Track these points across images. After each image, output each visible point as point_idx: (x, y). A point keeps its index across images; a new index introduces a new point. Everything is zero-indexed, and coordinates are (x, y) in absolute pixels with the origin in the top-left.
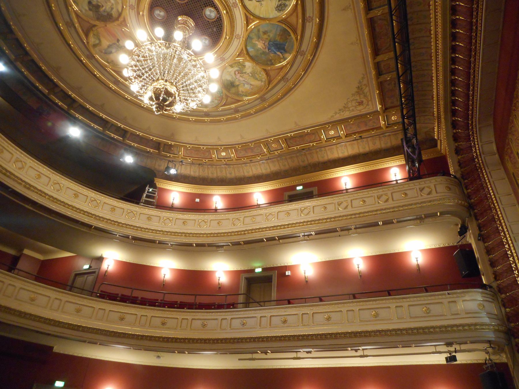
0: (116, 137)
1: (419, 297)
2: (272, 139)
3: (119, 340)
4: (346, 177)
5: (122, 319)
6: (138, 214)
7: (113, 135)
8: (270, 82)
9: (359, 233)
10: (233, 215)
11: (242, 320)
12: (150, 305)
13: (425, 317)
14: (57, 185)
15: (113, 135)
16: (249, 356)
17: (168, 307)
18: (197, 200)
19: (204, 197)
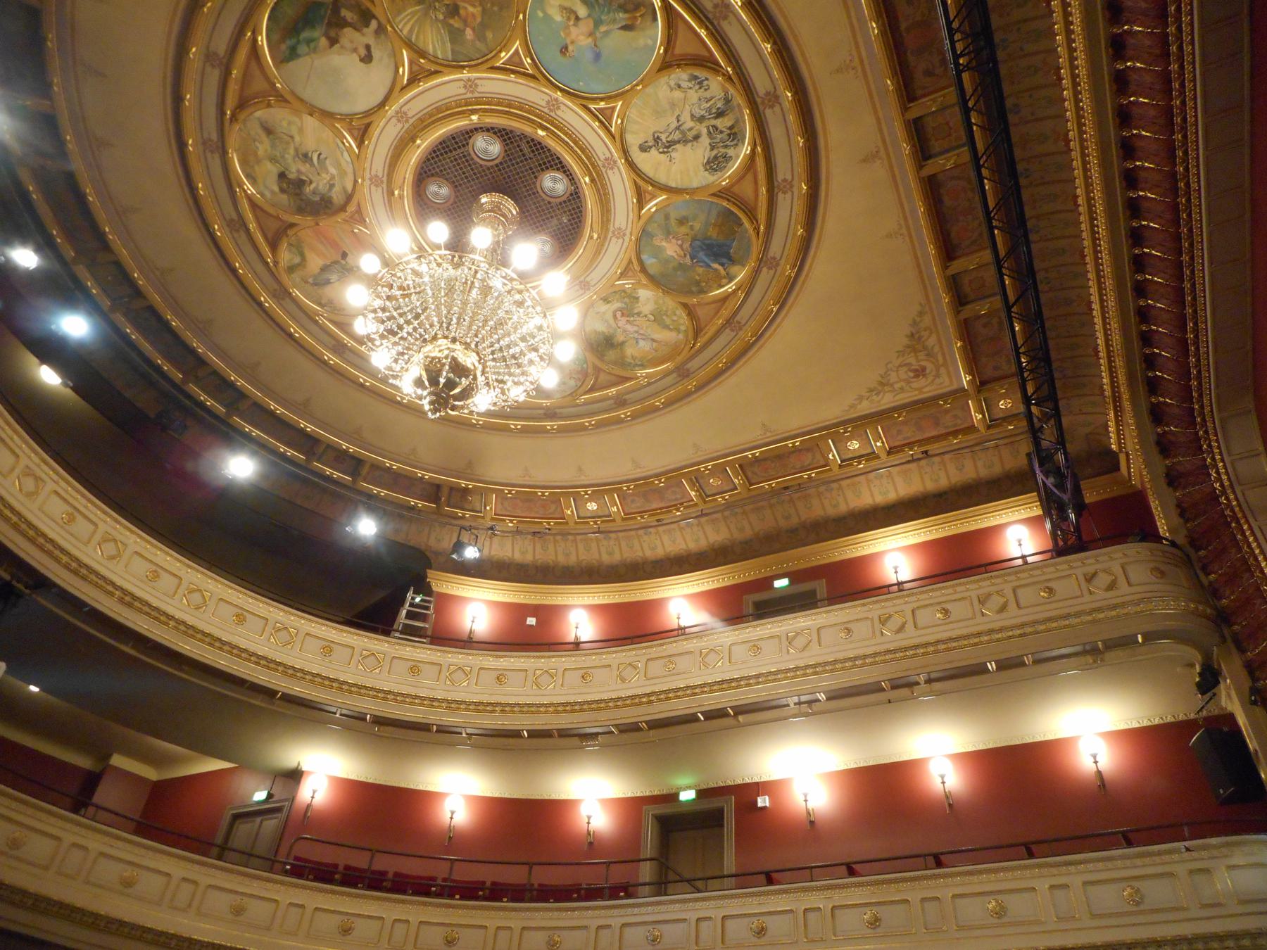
4: (895, 553)
7: (328, 471)
9: (939, 694)
15: (328, 471)
18: (531, 621)
19: (548, 614)
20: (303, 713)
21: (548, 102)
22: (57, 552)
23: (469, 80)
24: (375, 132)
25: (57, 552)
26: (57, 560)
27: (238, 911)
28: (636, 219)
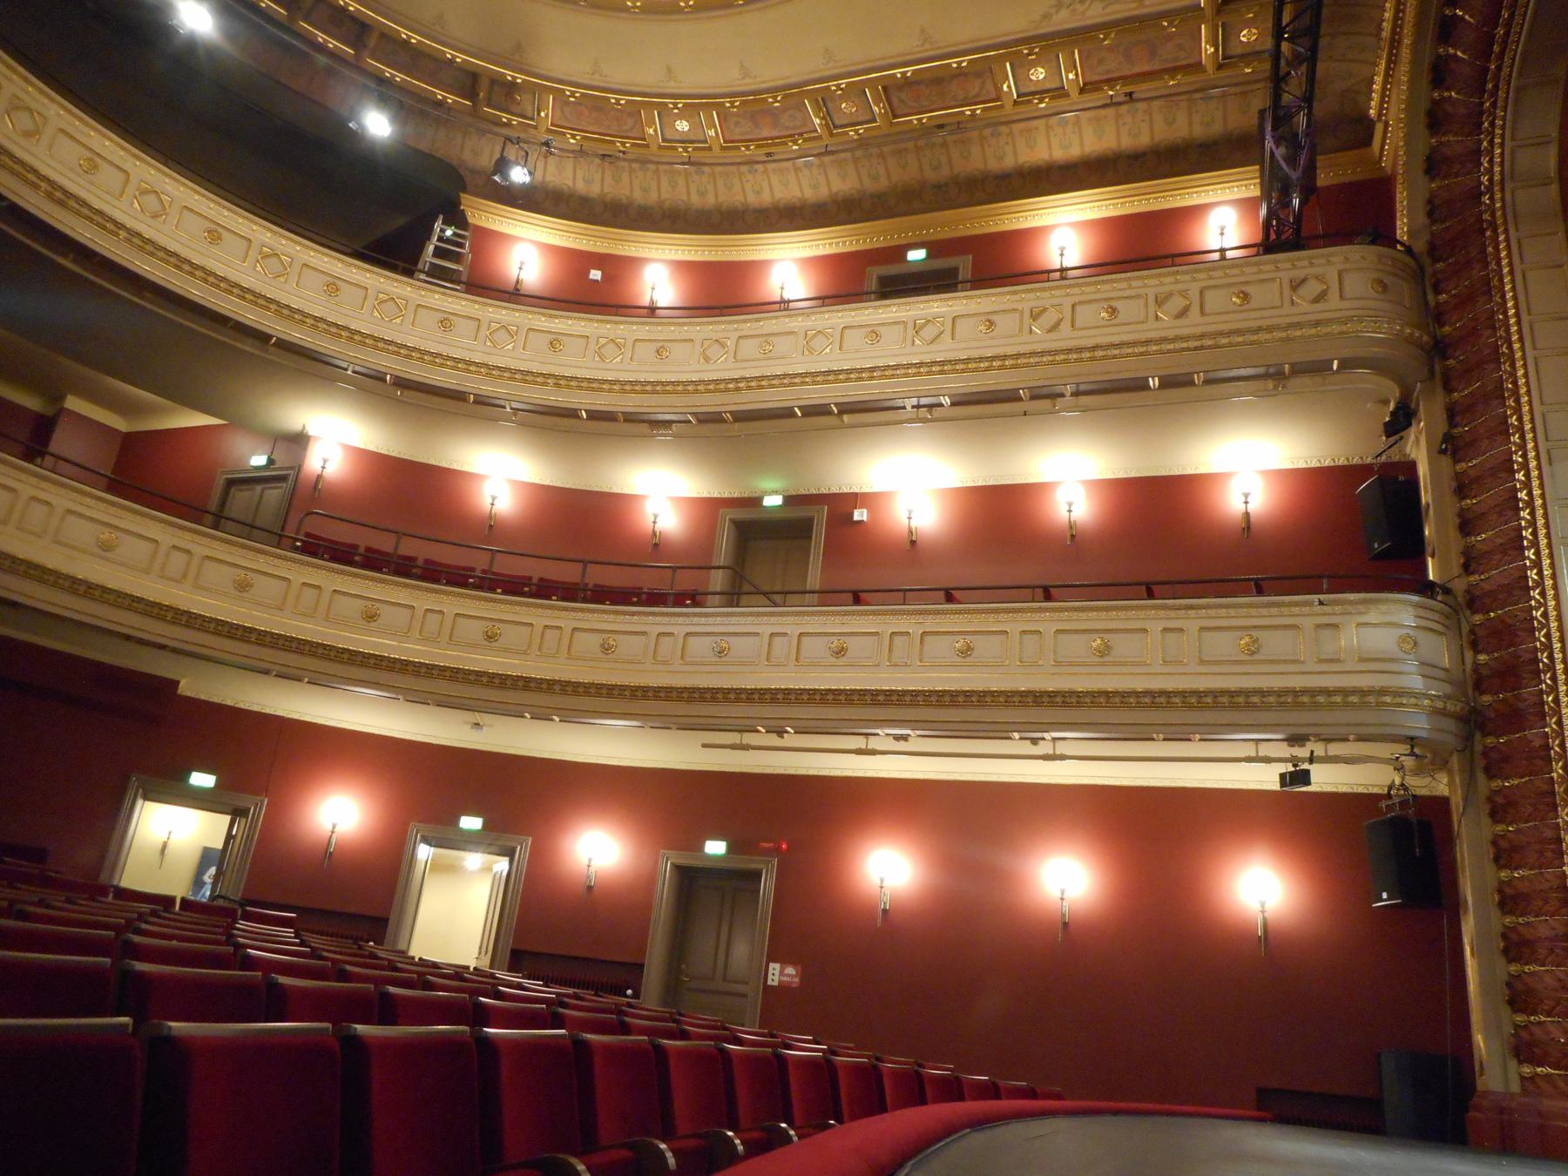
1: (1283, 604)
5: (490, 637)
6: (411, 308)
12: (450, 583)
14: (152, 197)
16: (733, 738)
18: (596, 275)
20: (307, 365)
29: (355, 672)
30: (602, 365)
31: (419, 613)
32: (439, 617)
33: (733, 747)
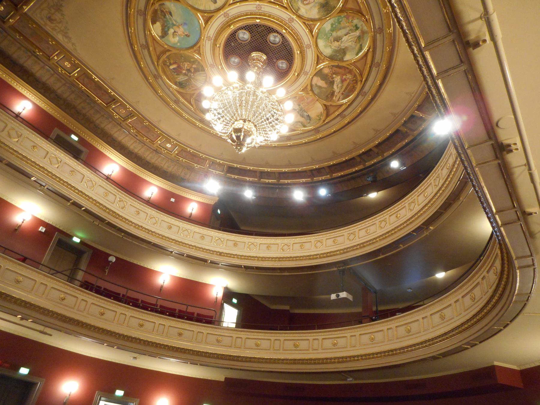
0: (270, 181)
2: (131, 109)
3: (175, 354)
5: (141, 326)
6: (258, 245)
7: (267, 181)
8: (328, 115)
10: (121, 195)
11: (295, 341)
13: (408, 336)
15: (267, 181)
16: (41, 328)
17: (114, 299)
18: (173, 200)
19: (180, 200)
20: (159, 250)
21: (256, 7)
22: (335, 253)
23: (259, 5)
24: (213, 20)
25: (335, 253)
26: (337, 255)
27: (180, 334)
28: (314, 69)
29: (170, 353)
30: (284, 252)
31: (89, 303)
32: (163, 326)
33: (41, 332)
